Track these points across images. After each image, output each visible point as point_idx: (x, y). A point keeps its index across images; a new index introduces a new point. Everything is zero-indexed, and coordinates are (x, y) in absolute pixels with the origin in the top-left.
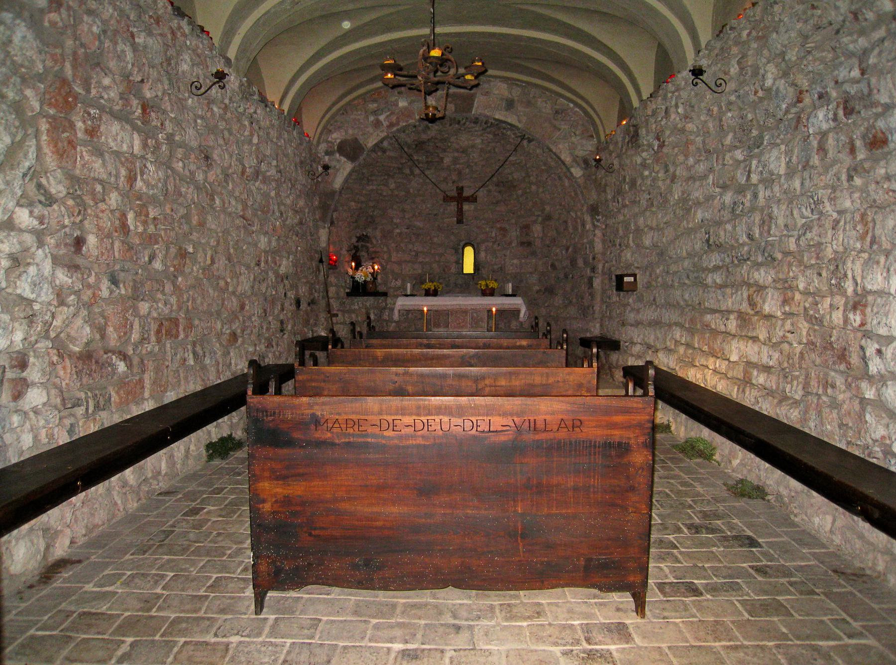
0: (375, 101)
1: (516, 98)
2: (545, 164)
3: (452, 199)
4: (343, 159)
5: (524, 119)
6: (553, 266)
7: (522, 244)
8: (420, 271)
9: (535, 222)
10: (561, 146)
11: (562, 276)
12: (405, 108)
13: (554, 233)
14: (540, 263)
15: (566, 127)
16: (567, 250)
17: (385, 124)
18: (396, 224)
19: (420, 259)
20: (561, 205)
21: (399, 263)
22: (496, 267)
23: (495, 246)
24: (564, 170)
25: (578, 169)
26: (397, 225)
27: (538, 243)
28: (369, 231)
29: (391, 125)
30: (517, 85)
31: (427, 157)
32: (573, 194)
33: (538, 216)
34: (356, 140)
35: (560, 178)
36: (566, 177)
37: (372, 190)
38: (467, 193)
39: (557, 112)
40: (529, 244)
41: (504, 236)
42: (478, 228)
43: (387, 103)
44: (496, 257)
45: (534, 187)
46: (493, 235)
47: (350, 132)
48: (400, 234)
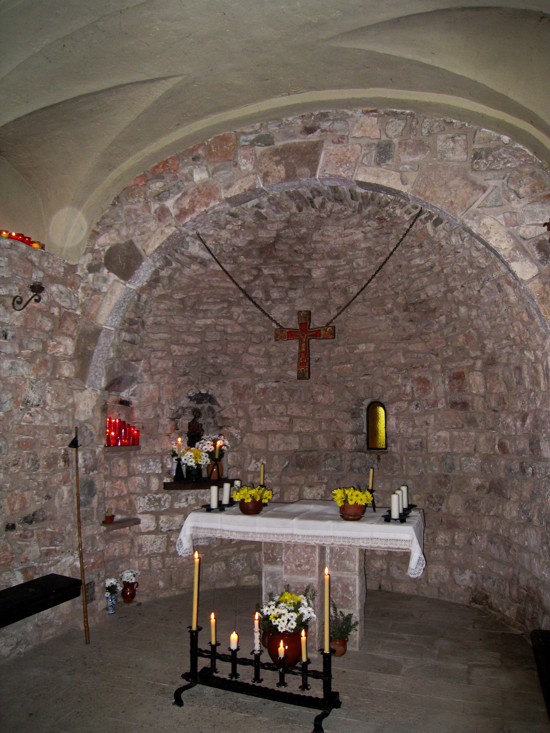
0: (160, 177)
1: (396, 141)
2: (471, 264)
3: (291, 334)
4: (113, 277)
5: (412, 177)
6: (502, 446)
7: (454, 405)
8: (296, 447)
9: (472, 368)
10: (488, 221)
11: (516, 467)
12: (205, 184)
13: (503, 389)
14: (482, 439)
15: (499, 183)
16: (524, 420)
17: (174, 211)
18: (258, 375)
19: (297, 429)
20: (508, 338)
21: (264, 434)
22: (413, 442)
23: (412, 407)
24: (503, 269)
25: (528, 263)
26: (261, 379)
27: (478, 404)
28: (212, 388)
29: (183, 213)
30: (395, 114)
31: (285, 270)
32: (526, 318)
33: (476, 358)
34: (131, 244)
35: (500, 287)
36: (509, 283)
37: (207, 327)
38: (316, 322)
39: (477, 156)
40: (464, 405)
41: (425, 391)
42: (385, 378)
43: (176, 178)
44: (414, 426)
45: (463, 310)
46: (408, 389)
47: (124, 232)
48: (264, 390)
